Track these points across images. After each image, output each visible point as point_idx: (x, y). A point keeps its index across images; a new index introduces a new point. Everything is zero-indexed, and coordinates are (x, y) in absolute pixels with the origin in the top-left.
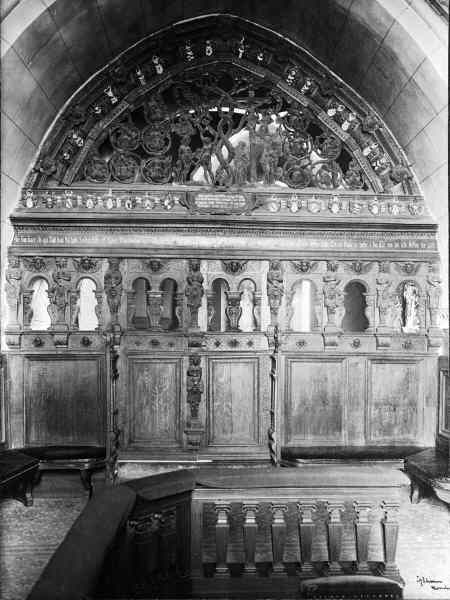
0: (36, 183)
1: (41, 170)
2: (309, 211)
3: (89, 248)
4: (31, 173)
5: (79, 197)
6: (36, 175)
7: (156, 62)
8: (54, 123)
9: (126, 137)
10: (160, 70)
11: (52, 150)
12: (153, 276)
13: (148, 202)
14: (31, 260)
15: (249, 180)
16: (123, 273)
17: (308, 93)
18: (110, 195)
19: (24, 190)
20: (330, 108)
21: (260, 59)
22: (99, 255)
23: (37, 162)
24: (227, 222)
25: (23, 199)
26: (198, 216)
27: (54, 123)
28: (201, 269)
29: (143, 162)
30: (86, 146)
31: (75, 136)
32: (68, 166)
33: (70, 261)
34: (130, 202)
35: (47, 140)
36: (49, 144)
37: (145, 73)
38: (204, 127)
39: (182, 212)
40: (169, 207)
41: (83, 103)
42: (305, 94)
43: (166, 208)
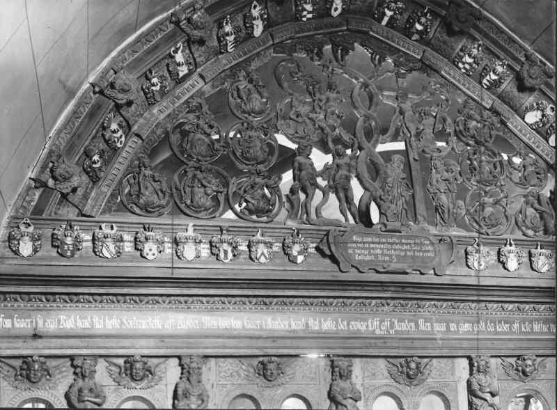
0: (38, 210)
1: (51, 183)
2: (505, 268)
3: (207, 337)
4: (29, 188)
5: (127, 237)
6: (38, 193)
7: (255, 13)
8: (165, 15)
9: (199, 136)
10: (258, 31)
11: (71, 148)
12: (267, 392)
13: (262, 249)
14: (17, 363)
15: (415, 220)
16: (208, 387)
17: (494, 85)
18: (190, 233)
19: (15, 222)
20: (532, 109)
21: (231, 135)
22: (162, 352)
23: (44, 168)
24: (403, 286)
25: (10, 238)
26: (352, 275)
27: (165, 15)
28: (353, 376)
29: (233, 181)
30: (129, 148)
31: (114, 126)
32: (94, 183)
33: (101, 366)
34: (229, 249)
35: (65, 126)
36: (65, 137)
37: (237, 30)
38: (334, 128)
39: (324, 269)
40: (300, 259)
41: (132, 67)
42: (488, 89)
43: (293, 261)
